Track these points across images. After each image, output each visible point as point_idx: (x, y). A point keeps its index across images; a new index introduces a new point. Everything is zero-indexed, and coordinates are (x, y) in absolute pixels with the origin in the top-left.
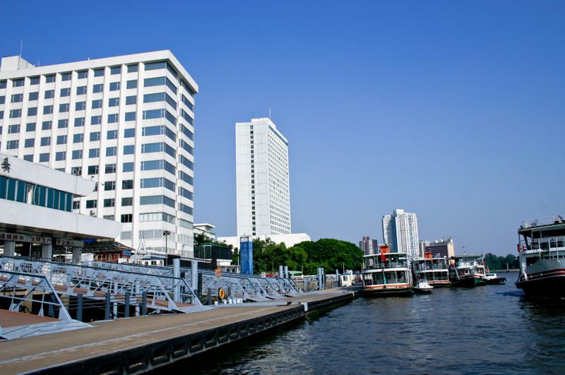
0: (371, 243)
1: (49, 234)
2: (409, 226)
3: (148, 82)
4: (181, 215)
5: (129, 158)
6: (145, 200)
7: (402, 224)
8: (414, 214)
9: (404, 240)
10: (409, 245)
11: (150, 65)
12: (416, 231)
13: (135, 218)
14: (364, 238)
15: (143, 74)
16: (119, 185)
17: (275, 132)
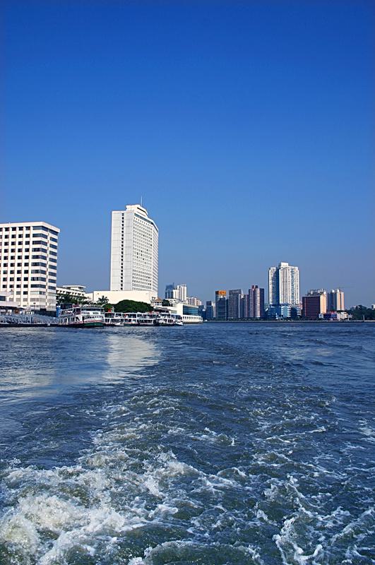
0: (258, 291)
1: (99, 325)
2: (291, 278)
3: (35, 236)
4: (49, 291)
5: (27, 254)
6: (32, 286)
7: (285, 276)
8: (297, 268)
9: (285, 290)
10: (290, 294)
11: (35, 228)
12: (297, 283)
13: (29, 293)
14: (253, 287)
15: (32, 232)
16: (24, 250)
17: (149, 221)
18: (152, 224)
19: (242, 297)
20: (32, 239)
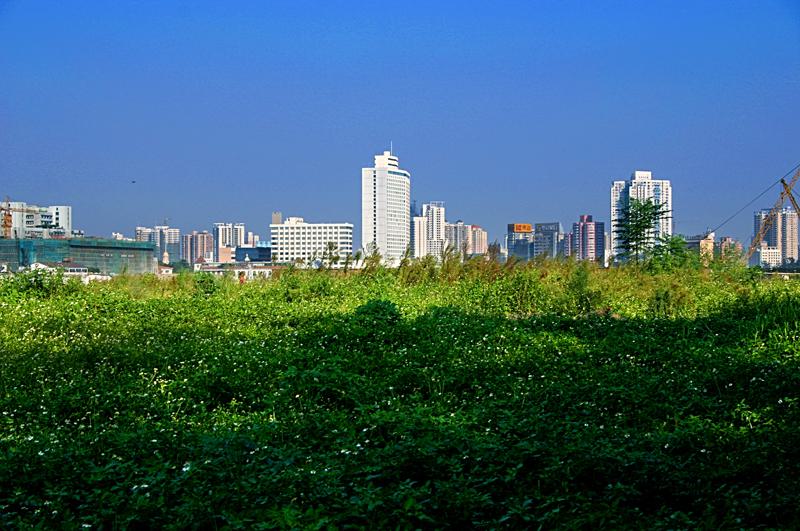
0: (592, 227)
11: (341, 228)
15: (340, 230)
17: (401, 174)
18: (405, 175)
19: (561, 237)
20: (339, 236)
